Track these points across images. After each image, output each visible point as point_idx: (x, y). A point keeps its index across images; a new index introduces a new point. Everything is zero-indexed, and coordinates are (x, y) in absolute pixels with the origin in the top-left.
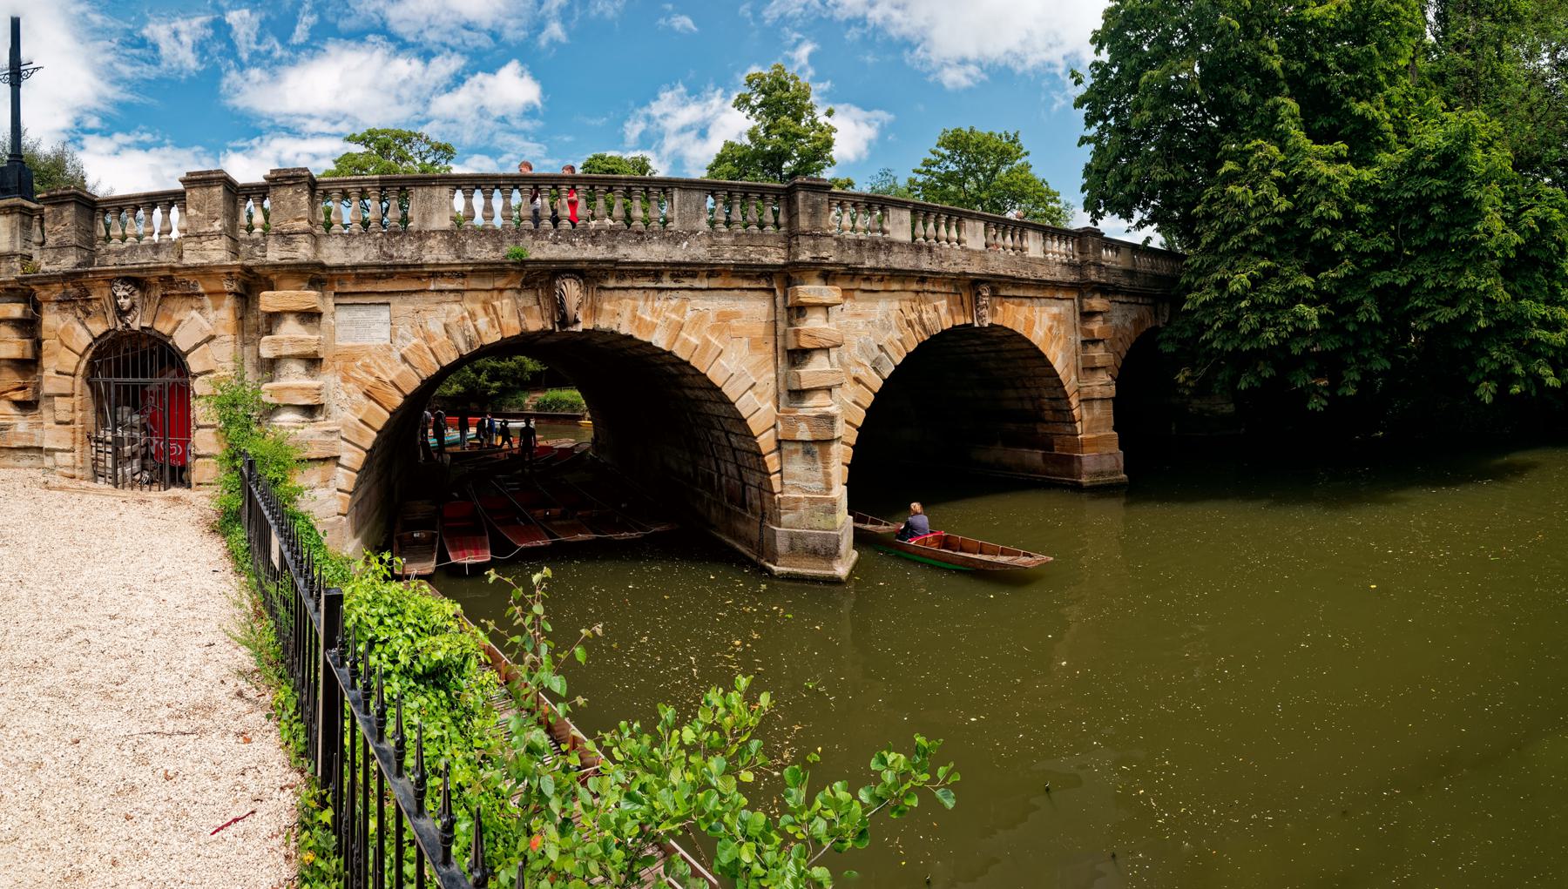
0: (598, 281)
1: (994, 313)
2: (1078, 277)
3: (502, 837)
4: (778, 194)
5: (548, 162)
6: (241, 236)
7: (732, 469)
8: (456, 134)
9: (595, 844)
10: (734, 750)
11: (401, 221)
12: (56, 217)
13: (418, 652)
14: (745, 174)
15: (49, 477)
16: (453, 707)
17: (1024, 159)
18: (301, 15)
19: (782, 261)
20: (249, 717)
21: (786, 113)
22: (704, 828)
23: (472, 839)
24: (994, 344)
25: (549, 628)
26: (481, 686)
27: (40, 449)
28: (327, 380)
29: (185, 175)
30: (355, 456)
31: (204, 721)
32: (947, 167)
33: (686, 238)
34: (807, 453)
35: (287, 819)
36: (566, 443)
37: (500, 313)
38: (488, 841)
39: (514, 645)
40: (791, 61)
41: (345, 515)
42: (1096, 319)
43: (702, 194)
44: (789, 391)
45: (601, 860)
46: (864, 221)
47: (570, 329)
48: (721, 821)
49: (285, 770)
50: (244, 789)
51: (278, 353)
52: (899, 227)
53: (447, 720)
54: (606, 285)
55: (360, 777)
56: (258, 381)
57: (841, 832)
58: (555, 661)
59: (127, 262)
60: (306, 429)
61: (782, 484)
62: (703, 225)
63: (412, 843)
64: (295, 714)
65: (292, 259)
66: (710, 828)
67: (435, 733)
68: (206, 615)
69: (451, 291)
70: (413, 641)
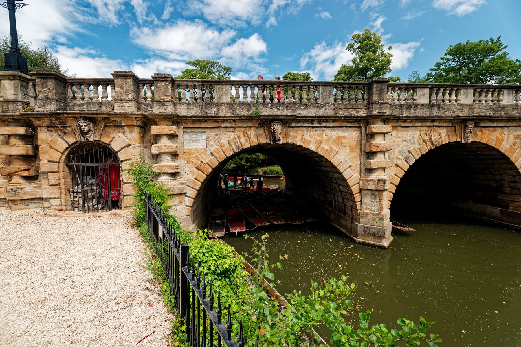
0: (288, 124)
1: (475, 135)
3: (249, 329)
4: (364, 86)
5: (269, 76)
6: (141, 102)
7: (340, 199)
8: (232, 63)
9: (284, 333)
11: (210, 99)
12: (43, 84)
14: (350, 78)
15: (47, 211)
16: (231, 284)
17: (503, 51)
18: (166, 7)
19: (365, 115)
20: (151, 297)
23: (239, 331)
25: (268, 256)
27: (41, 199)
28: (181, 162)
29: (113, 72)
30: (193, 192)
31: (131, 302)
32: (450, 65)
33: (324, 106)
34: (372, 194)
35: (168, 332)
36: (275, 187)
37: (250, 136)
38: (244, 331)
39: (254, 262)
40: (373, 27)
41: (189, 215)
43: (332, 88)
44: (366, 169)
45: (286, 339)
46: (404, 95)
47: (277, 143)
48: (334, 325)
49: (166, 314)
50: (150, 324)
51: (159, 152)
53: (229, 289)
54: (291, 125)
55: (196, 312)
56: (151, 163)
58: (270, 268)
59: (85, 110)
60: (172, 182)
61: (361, 206)
62: (331, 100)
63: (216, 333)
64: (170, 293)
65: (165, 112)
66: (330, 327)
67: (224, 294)
68: (131, 260)
69: (230, 127)
70: (216, 261)
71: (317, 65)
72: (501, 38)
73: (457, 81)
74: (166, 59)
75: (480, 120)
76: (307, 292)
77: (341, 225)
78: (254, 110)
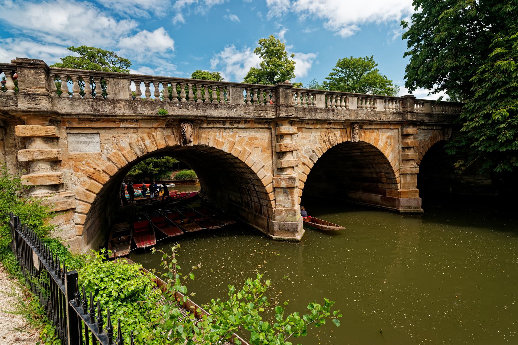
0: (199, 125)
1: (360, 136)
2: (401, 119)
5: (178, 73)
7: (256, 199)
10: (257, 300)
13: (122, 289)
14: (260, 81)
17: (375, 68)
19: (274, 117)
21: (275, 56)
22: (246, 328)
24: (360, 149)
25: (179, 268)
26: (154, 297)
30: (84, 207)
32: (340, 75)
33: (235, 107)
34: (285, 192)
36: (189, 192)
41: (81, 236)
42: (410, 137)
43: (241, 89)
44: (277, 168)
47: (188, 145)
48: (252, 325)
51: (31, 159)
52: (320, 102)
53: (137, 314)
54: (202, 126)
57: (296, 330)
61: (276, 204)
62: (242, 102)
64: (54, 336)
66: (248, 328)
69: (131, 128)
70: (119, 285)
71: (227, 68)
72: (374, 58)
73: (346, 90)
74: (39, 41)
75: (363, 123)
76: (225, 298)
77: (258, 225)
78: (160, 109)
